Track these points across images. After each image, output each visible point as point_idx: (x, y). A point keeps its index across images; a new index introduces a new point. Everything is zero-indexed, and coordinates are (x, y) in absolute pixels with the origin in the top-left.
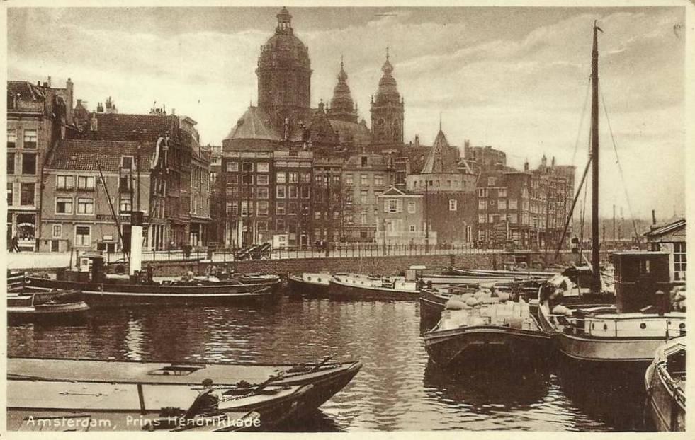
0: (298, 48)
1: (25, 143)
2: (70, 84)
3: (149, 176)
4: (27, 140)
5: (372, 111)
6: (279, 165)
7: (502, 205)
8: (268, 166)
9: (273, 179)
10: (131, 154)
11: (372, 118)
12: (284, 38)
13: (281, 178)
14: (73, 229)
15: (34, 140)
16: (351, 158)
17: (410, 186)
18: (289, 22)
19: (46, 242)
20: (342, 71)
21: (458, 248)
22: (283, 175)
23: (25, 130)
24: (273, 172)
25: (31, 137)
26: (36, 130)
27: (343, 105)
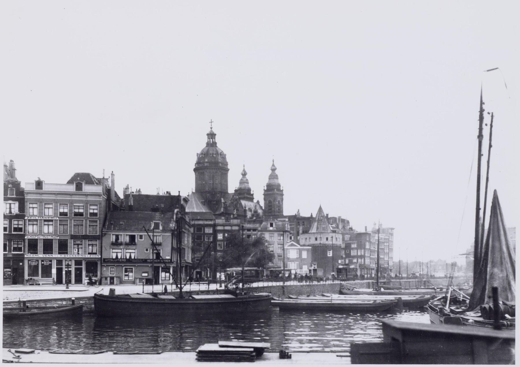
0: (221, 155)
1: (60, 213)
2: (39, 178)
3: (170, 234)
4: (92, 211)
5: (264, 195)
6: (219, 228)
7: (353, 253)
8: (212, 229)
9: (215, 237)
10: (159, 220)
11: (265, 199)
12: (211, 148)
13: (220, 237)
14: (122, 269)
15: (95, 211)
16: (264, 223)
17: (302, 242)
18: (215, 138)
19: (106, 278)
20: (244, 170)
21: (48, 247)
22: (221, 235)
23: (45, 204)
24: (215, 233)
25: (94, 209)
26: (97, 205)
27: (245, 193)
